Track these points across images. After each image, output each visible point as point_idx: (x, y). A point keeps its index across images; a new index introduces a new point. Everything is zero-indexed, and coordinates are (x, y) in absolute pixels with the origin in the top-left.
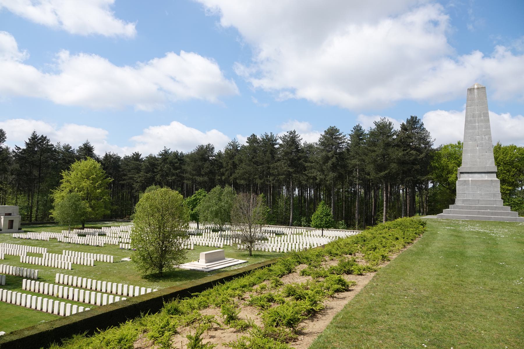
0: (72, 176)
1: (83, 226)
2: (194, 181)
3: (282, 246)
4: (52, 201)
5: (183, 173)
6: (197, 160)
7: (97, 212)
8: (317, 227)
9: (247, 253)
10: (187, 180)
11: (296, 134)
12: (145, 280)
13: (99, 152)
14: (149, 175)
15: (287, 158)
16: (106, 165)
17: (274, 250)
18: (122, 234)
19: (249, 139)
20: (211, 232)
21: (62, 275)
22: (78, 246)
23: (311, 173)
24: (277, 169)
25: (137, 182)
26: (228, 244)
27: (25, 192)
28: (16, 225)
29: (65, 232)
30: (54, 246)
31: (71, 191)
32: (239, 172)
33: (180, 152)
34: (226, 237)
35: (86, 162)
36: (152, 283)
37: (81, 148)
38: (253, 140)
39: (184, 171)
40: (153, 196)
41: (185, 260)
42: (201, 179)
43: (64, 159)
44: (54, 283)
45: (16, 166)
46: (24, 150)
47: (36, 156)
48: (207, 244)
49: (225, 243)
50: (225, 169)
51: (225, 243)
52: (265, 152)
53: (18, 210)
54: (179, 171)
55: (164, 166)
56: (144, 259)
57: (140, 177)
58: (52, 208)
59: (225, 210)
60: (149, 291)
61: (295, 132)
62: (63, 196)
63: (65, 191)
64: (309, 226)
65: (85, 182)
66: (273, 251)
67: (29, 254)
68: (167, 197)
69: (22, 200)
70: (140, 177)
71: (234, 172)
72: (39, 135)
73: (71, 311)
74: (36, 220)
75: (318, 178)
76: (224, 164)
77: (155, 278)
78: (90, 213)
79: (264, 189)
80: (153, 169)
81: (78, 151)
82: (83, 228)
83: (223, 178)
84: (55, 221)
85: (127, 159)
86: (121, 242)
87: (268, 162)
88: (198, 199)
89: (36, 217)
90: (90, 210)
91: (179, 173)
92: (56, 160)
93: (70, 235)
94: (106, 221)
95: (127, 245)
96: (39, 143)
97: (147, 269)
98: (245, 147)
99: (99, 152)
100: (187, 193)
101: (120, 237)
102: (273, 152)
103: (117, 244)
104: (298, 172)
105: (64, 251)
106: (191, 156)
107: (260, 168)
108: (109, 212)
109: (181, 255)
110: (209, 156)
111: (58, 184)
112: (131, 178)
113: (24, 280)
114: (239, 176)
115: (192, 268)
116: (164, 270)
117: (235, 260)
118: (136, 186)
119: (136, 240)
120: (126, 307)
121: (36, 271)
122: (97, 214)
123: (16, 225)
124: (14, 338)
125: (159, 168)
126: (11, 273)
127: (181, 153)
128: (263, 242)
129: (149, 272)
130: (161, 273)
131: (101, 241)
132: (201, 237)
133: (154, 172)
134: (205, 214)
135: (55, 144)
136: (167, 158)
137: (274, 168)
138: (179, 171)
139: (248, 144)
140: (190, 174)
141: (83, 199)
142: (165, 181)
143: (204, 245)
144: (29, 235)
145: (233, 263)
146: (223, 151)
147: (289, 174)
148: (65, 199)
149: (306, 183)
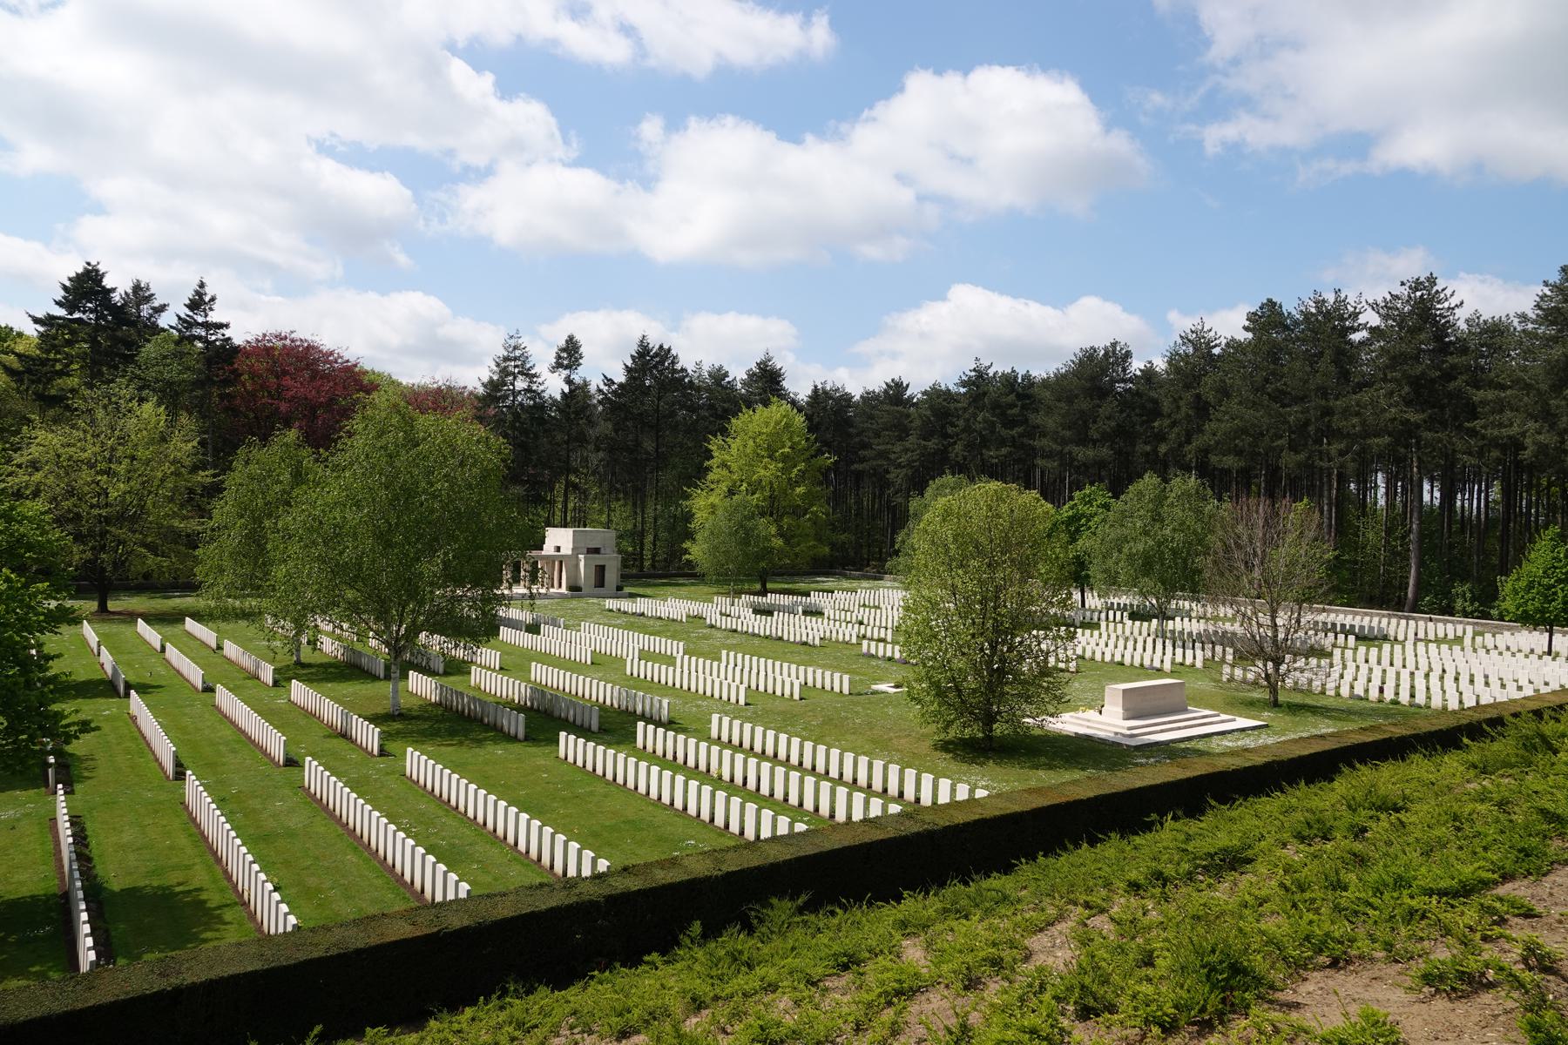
0: (734, 451)
1: (764, 585)
2: (1067, 461)
3: (1362, 680)
4: (689, 517)
5: (1031, 436)
6: (1077, 396)
7: (797, 549)
8: (1528, 620)
9: (1261, 694)
10: (1043, 457)
11: (1438, 288)
12: (944, 755)
13: (799, 386)
14: (932, 444)
15: (1397, 375)
16: (816, 419)
17: (1359, 691)
18: (865, 614)
19: (1252, 317)
20: (1126, 620)
21: (726, 720)
22: (756, 641)
23: (1501, 425)
24: (1358, 414)
25: (899, 466)
26: (1189, 661)
27: (626, 493)
28: (612, 577)
29: (722, 602)
30: (702, 640)
31: (731, 492)
32: (1217, 428)
33: (1021, 372)
34: (1183, 640)
35: (766, 412)
36: (965, 767)
37: (751, 375)
38: (1268, 319)
39: (1034, 431)
40: (953, 507)
41: (1062, 702)
42: (1091, 453)
43: (711, 407)
44: (708, 739)
45: (605, 428)
46: (621, 385)
47: (647, 400)
48: (1118, 658)
49: (1179, 659)
50: (1167, 422)
51: (1179, 659)
52: (1313, 359)
53: (614, 542)
54: (1020, 429)
55: (975, 416)
56: (941, 693)
57: (906, 450)
58: (690, 536)
59: (1174, 552)
60: (962, 793)
61: (1432, 280)
62: (713, 506)
63: (718, 491)
64: (1487, 616)
65: (766, 468)
66: (1352, 696)
67: (645, 655)
68: (1004, 508)
69: (621, 512)
70: (906, 450)
71: (1200, 430)
72: (654, 343)
73: (774, 827)
74: (653, 566)
75: (1528, 441)
76: (1166, 405)
77: (979, 749)
78: (780, 551)
79: (1303, 484)
80: (943, 427)
81: (744, 383)
82: (763, 593)
83: (1163, 449)
84: (698, 570)
85: (869, 398)
86: (864, 637)
87: (1323, 392)
88: (1083, 515)
89: (653, 558)
90: (778, 542)
91: (1021, 435)
92: (693, 409)
93: (734, 610)
94: (819, 575)
95: (881, 645)
96: (655, 367)
97: (949, 724)
98: (1240, 344)
99: (799, 386)
100: (1052, 493)
101: (861, 623)
102: (1345, 355)
103: (854, 640)
104: (1444, 425)
105: (724, 652)
106: (1058, 384)
107: (1294, 413)
108: (827, 549)
109: (1048, 686)
110: (1113, 381)
111: (703, 472)
112: (883, 455)
113: (641, 724)
114: (1217, 443)
115: (1082, 731)
116: (999, 729)
117: (1224, 717)
118: (897, 476)
119: (914, 634)
120: (906, 837)
121: (665, 702)
122: (796, 555)
123: (612, 577)
124: (633, 884)
125: (961, 423)
126: (608, 702)
127: (1027, 377)
128: (1313, 661)
129: (952, 733)
130: (989, 738)
131: (812, 629)
132: (1096, 633)
133: (946, 436)
134: (1110, 563)
135: (690, 368)
136: (985, 394)
137: (1346, 413)
138: (1020, 429)
139: (1250, 335)
140: (1055, 441)
141: (762, 514)
142: (978, 461)
143: (1108, 658)
144: (641, 605)
145: (1222, 729)
146: (1160, 364)
147: (1406, 433)
148: (720, 512)
149: (1474, 461)
